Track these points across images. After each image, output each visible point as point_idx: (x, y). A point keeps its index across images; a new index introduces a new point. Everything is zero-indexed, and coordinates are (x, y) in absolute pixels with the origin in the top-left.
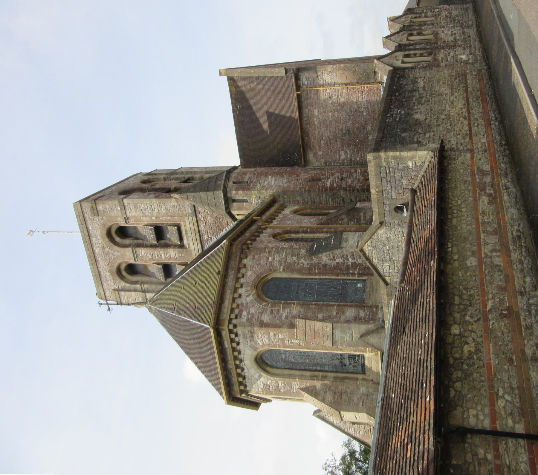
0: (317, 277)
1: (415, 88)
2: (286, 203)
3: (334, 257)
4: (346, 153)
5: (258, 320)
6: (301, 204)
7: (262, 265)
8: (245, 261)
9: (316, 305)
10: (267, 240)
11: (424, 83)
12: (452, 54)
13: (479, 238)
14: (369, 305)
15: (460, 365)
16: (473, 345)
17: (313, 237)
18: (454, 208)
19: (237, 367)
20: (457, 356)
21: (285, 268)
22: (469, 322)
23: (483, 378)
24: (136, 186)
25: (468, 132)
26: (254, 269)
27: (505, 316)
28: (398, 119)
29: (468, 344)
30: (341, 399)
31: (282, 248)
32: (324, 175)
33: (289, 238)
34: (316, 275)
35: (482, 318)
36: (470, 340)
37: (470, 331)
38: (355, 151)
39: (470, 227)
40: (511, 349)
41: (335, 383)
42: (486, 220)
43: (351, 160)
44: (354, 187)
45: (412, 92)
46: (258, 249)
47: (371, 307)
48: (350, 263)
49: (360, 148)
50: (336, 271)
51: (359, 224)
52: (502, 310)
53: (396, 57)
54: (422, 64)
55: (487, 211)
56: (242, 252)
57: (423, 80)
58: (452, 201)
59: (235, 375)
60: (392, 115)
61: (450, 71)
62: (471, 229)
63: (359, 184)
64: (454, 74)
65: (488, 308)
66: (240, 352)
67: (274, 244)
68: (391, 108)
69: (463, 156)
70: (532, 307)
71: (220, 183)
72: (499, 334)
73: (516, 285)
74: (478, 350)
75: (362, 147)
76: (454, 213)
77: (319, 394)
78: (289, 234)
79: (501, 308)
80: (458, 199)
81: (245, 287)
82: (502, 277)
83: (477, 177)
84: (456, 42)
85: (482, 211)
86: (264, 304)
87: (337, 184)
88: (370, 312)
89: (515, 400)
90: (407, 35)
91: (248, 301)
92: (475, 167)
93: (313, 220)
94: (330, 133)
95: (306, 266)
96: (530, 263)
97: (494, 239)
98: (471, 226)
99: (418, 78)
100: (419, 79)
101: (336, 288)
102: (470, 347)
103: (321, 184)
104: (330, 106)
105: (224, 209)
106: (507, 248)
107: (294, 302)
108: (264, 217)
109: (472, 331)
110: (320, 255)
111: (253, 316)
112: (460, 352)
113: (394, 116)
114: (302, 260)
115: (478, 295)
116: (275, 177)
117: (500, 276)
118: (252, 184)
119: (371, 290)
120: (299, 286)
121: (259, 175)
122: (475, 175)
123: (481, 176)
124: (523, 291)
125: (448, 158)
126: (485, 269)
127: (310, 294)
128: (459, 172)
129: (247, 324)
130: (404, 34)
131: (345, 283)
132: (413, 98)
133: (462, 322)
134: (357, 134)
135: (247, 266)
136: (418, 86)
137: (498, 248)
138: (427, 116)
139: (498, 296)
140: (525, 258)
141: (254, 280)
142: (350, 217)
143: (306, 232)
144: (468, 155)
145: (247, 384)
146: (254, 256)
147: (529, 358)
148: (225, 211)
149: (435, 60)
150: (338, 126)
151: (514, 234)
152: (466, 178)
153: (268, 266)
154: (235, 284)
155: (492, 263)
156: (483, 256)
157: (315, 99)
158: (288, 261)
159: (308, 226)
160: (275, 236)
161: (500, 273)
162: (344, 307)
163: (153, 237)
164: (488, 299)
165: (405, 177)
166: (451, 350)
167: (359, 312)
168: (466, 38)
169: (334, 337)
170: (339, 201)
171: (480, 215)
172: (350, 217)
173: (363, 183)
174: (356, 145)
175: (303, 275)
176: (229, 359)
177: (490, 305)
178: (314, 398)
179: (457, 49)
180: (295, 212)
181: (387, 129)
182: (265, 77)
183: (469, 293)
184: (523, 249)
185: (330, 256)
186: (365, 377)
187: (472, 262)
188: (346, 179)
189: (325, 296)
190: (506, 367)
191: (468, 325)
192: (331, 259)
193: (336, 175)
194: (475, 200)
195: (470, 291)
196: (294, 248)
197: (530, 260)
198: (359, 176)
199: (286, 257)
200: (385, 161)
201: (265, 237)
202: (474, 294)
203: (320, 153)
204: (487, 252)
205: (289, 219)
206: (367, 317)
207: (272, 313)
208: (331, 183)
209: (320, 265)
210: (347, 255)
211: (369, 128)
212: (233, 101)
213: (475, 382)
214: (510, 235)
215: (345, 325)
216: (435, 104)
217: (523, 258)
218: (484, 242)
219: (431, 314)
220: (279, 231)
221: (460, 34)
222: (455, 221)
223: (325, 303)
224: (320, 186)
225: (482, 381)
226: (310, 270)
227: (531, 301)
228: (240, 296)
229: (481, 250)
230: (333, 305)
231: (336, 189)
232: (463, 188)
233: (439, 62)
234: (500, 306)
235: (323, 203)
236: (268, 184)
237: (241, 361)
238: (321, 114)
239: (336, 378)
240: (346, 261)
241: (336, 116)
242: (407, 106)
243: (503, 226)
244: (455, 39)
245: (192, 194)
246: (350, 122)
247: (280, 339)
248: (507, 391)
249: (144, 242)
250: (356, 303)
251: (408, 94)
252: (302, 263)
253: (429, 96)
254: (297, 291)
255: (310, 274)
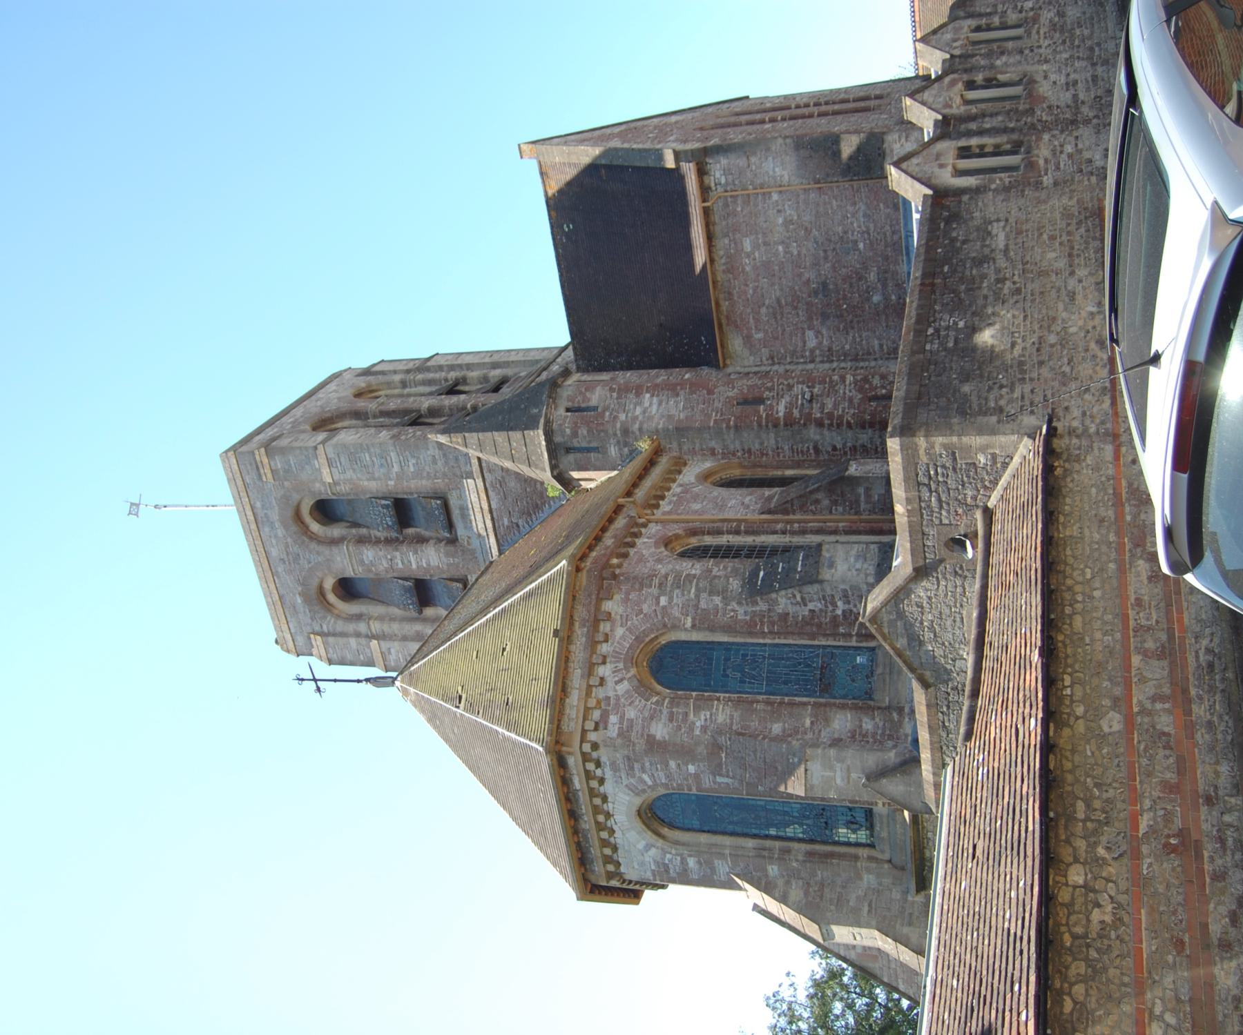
0: (768, 641)
1: (986, 251)
2: (685, 454)
3: (802, 598)
4: (818, 333)
5: (642, 735)
6: (720, 457)
7: (645, 615)
8: (608, 606)
9: (768, 703)
10: (652, 555)
11: (1007, 237)
12: (1069, 149)
13: (1128, 667)
14: (884, 705)
15: (1084, 949)
16: (1109, 908)
17: (753, 544)
18: (1078, 588)
19: (600, 827)
20: (1079, 930)
21: (697, 622)
22: (1103, 859)
23: (1126, 979)
24: (345, 406)
25: (1108, 385)
26: (629, 623)
27: (1174, 849)
28: (951, 345)
29: (1099, 905)
30: (821, 897)
31: (688, 575)
32: (771, 389)
33: (700, 547)
34: (764, 638)
35: (1129, 852)
36: (1104, 899)
37: (1104, 878)
38: (839, 330)
39: (1110, 638)
40: (1181, 921)
41: (808, 865)
42: (1144, 622)
43: (830, 349)
44: (840, 417)
45: (980, 262)
46: (635, 578)
47: (889, 708)
48: (839, 612)
49: (851, 322)
50: (808, 629)
51: (856, 513)
52: (1169, 836)
53: (938, 156)
54: (1001, 179)
55: (1146, 598)
56: (600, 588)
57: (1004, 227)
58: (1073, 569)
59: (597, 843)
60: (937, 331)
61: (1065, 200)
62: (1112, 644)
63: (852, 411)
64: (1075, 211)
65: (1141, 832)
66: (605, 799)
67: (670, 566)
68: (935, 311)
69: (1096, 451)
70: (1229, 833)
71: (536, 411)
72: (1161, 889)
73: (1200, 781)
74: (1118, 921)
75: (856, 320)
76: (1078, 602)
77: (776, 886)
78: (700, 537)
79: (1166, 831)
80: (1086, 566)
81: (610, 662)
82: (1171, 760)
83: (1127, 509)
84: (1077, 108)
85: (1137, 599)
86: (655, 699)
87: (801, 411)
88: (884, 720)
89: (1183, 1026)
90: (960, 86)
91: (620, 693)
92: (1124, 483)
93: (751, 500)
94: (781, 290)
95: (743, 617)
96: (1230, 731)
97: (1159, 671)
98: (1112, 635)
99: (990, 223)
100: (995, 224)
101: (809, 666)
102: (1104, 913)
103: (765, 410)
104: (781, 229)
105: (548, 469)
106: (1185, 691)
107: (718, 695)
108: (640, 493)
109: (1108, 880)
110: (774, 595)
111: (632, 727)
112: (1084, 922)
113: (943, 333)
114: (734, 605)
115: (1123, 801)
116: (658, 396)
117: (1167, 757)
118: (607, 414)
119: (888, 670)
120: (727, 659)
121: (624, 390)
122: (1123, 505)
123: (1135, 505)
124: (1213, 794)
125: (1065, 457)
126: (1139, 742)
127: (753, 677)
128: (1089, 493)
129: (619, 741)
130: (953, 83)
131: (831, 653)
132: (982, 282)
133: (1089, 860)
134: (844, 291)
135: (613, 615)
136: (993, 247)
137: (1166, 690)
138: (1016, 335)
139: (1163, 806)
140: (1220, 717)
141: (630, 648)
142: (834, 497)
143: (737, 532)
144: (1109, 449)
145: (620, 860)
146: (628, 594)
147: (1216, 942)
148: (549, 473)
149: (1031, 165)
150: (800, 275)
151: (1201, 658)
152: (1103, 513)
153: (660, 617)
154: (591, 656)
155: (1154, 727)
156: (1136, 709)
157: (744, 216)
158: (703, 605)
159: (739, 516)
160: (667, 543)
161: (1167, 752)
162: (828, 709)
163: (390, 523)
164: (1142, 810)
165: (970, 483)
166: (1068, 917)
167: (861, 721)
168: (1101, 98)
169: (809, 777)
170: (805, 449)
171: (1133, 609)
172: (834, 497)
173: (862, 409)
174: (842, 316)
175: (736, 637)
176: (584, 811)
177: (1144, 823)
178: (764, 895)
179: (1080, 132)
180: (705, 477)
181: (927, 372)
182: (628, 167)
183: (1105, 796)
184: (1218, 697)
185: (794, 596)
186: (873, 853)
187: (1113, 723)
188: (820, 399)
189: (786, 683)
190: (1170, 958)
191: (1101, 866)
192: (798, 603)
193: (797, 389)
194: (1122, 570)
195: (1107, 791)
196: (715, 577)
197: (1230, 724)
198: (850, 391)
199: (697, 596)
200: (927, 454)
201: (645, 545)
202: (1115, 797)
203: (760, 335)
204: (1145, 702)
205: (696, 498)
206: (880, 732)
207: (671, 720)
208: (786, 408)
209: (772, 614)
210: (833, 596)
211: (872, 276)
212: (553, 213)
213: (1112, 986)
214: (1191, 659)
215: (832, 752)
216: (1033, 301)
217: (1215, 719)
218: (1138, 677)
219: (1029, 842)
220: (677, 529)
221: (1087, 81)
222: (1078, 622)
223: (786, 699)
224: (761, 417)
225: (1125, 985)
226: (750, 628)
227: (1227, 818)
228: (602, 681)
229: (1130, 697)
230: (805, 704)
231: (799, 423)
232: (1097, 536)
233: (1040, 172)
234: (1165, 826)
235: (770, 453)
236: (644, 412)
237: (608, 815)
238: (759, 249)
239: (810, 854)
240: (831, 608)
241: (795, 253)
242: (970, 305)
243: (1179, 637)
244: (1075, 96)
245: (475, 434)
246: (829, 265)
247: (691, 774)
248: (1170, 1006)
249: (372, 532)
250: (854, 698)
251: (972, 269)
252: (733, 610)
253: (1019, 275)
254: (724, 670)
255: (751, 634)
